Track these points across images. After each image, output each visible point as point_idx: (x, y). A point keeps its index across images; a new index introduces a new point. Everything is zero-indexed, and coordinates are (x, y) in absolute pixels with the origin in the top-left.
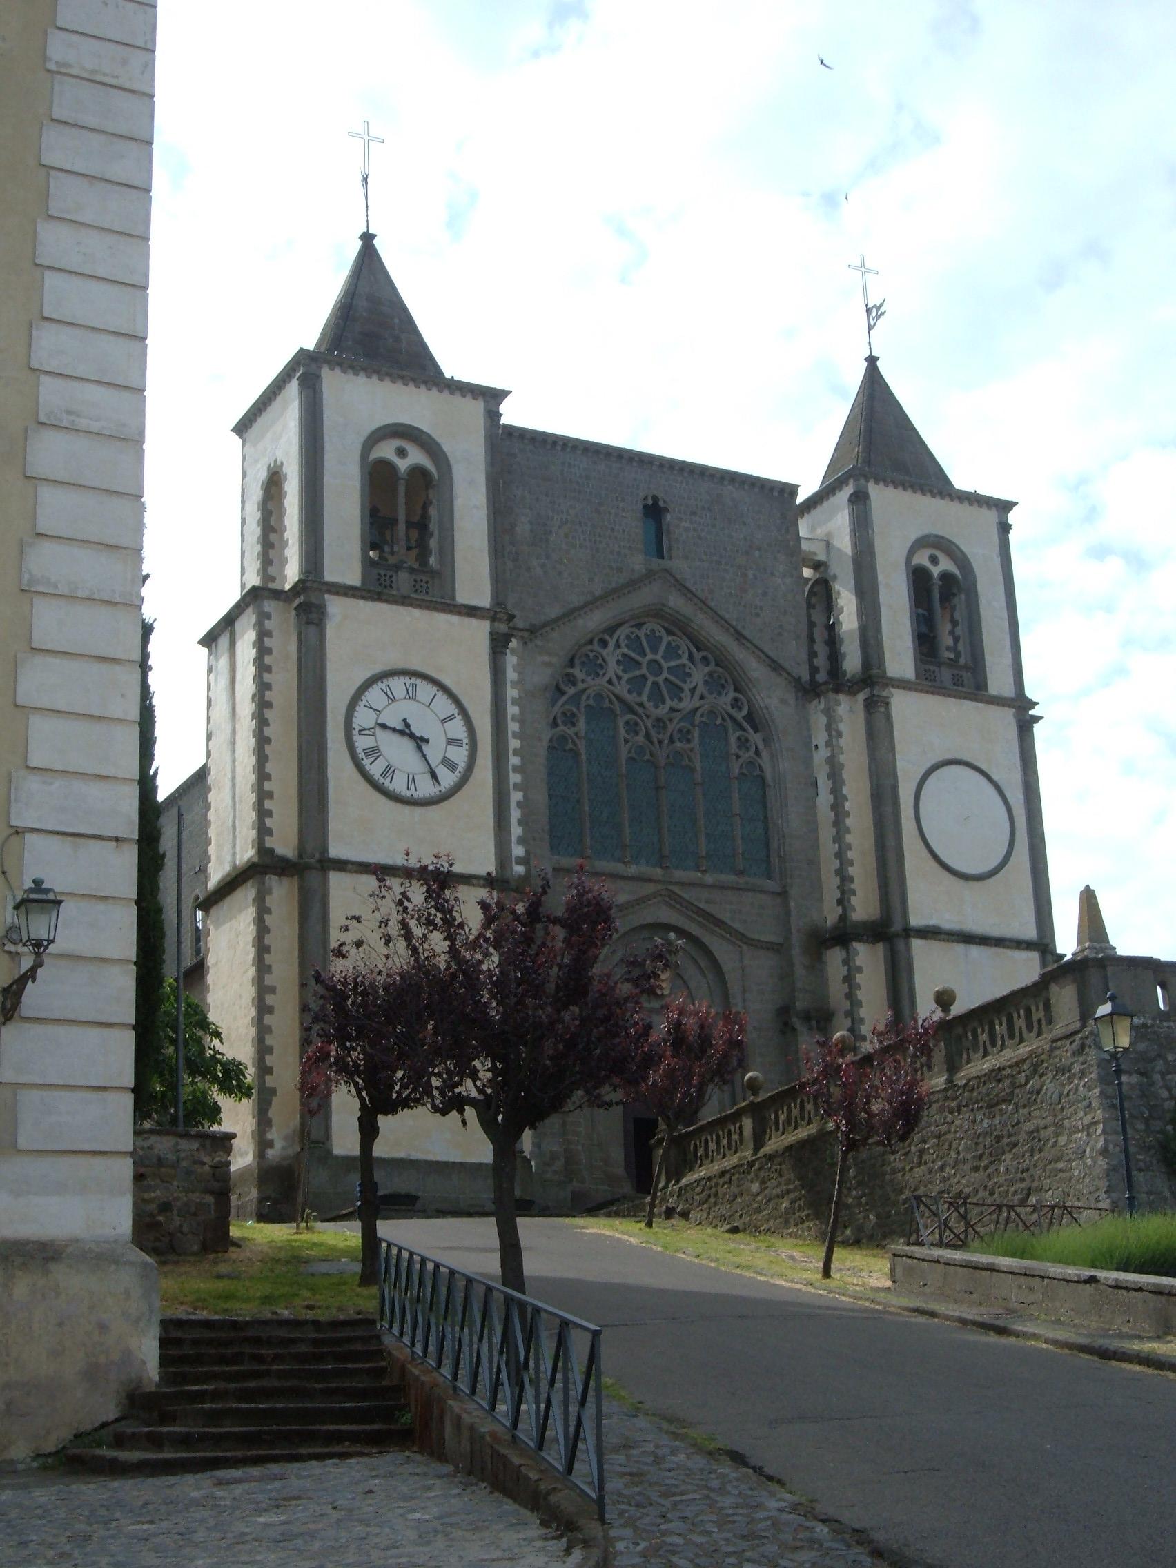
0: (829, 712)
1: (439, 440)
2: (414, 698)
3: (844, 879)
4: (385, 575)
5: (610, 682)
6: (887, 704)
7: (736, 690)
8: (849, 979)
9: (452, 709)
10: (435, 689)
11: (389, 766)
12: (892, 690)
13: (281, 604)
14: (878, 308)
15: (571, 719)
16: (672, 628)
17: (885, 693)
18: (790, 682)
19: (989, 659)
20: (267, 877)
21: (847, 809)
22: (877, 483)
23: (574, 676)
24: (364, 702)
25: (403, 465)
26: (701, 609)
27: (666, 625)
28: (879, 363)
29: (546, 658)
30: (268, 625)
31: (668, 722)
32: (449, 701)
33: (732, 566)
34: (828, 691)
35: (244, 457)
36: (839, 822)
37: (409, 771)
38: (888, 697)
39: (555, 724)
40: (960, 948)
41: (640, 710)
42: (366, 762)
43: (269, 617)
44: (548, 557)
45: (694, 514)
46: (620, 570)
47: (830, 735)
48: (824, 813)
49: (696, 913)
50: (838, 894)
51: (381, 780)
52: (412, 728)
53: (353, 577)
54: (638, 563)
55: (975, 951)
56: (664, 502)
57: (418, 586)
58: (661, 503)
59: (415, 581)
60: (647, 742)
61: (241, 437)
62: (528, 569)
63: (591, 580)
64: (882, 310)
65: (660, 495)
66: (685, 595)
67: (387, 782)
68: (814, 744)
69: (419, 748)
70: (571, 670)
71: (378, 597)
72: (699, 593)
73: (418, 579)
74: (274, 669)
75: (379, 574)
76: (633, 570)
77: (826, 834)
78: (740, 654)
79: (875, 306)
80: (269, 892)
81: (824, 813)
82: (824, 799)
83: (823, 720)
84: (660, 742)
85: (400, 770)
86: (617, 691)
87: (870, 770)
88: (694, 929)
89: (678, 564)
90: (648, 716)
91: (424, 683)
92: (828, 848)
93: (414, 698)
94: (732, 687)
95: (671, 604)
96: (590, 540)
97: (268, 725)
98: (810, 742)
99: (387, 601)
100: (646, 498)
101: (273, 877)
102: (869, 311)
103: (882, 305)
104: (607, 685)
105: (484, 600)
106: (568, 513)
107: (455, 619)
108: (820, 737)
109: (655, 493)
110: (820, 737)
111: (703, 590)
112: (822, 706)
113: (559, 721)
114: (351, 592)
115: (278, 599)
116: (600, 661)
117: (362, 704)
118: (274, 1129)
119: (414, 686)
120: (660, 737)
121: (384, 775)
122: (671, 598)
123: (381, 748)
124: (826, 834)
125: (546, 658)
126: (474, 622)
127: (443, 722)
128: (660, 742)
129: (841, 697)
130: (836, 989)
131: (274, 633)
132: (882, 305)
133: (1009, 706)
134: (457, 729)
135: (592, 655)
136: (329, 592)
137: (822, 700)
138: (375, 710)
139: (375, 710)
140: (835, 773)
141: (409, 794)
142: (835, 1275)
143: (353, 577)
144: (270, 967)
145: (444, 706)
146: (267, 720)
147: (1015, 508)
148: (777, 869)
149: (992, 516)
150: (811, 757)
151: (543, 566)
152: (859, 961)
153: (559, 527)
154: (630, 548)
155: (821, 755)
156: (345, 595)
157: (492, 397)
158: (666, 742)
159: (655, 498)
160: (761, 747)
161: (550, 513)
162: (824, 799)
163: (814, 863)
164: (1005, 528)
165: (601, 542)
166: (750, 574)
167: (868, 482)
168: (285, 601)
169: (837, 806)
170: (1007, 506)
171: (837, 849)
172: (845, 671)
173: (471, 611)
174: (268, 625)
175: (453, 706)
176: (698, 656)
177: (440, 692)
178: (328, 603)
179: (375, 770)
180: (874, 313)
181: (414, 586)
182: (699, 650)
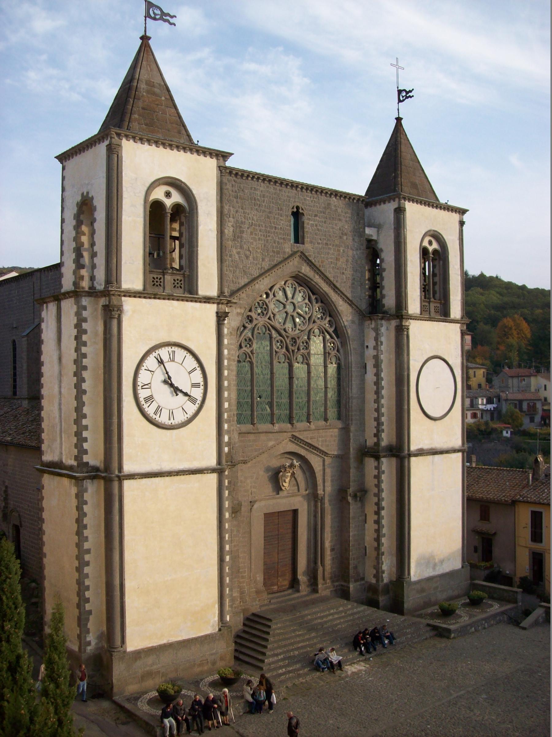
0: (377, 330)
1: (191, 187)
2: (173, 361)
3: (379, 424)
4: (157, 278)
5: (269, 318)
6: (408, 329)
7: (330, 316)
8: (378, 477)
9: (195, 364)
10: (186, 352)
11: (159, 407)
12: (411, 321)
13: (93, 298)
14: (407, 92)
15: (249, 341)
16: (300, 283)
17: (407, 324)
18: (357, 311)
19: (452, 297)
20: (85, 481)
21: (383, 385)
22: (409, 202)
23: (251, 317)
24: (145, 367)
25: (168, 203)
26: (317, 273)
27: (298, 281)
28: (403, 122)
29: (239, 310)
30: (85, 314)
31: (297, 339)
32: (193, 359)
33: (333, 245)
34: (377, 319)
35: (63, 178)
36: (377, 392)
37: (170, 409)
38: (409, 326)
39: (241, 347)
40: (430, 458)
41: (283, 333)
42: (145, 406)
43: (85, 308)
44: (241, 247)
45: (316, 216)
46: (278, 253)
47: (377, 344)
48: (370, 387)
49: (305, 445)
50: (375, 431)
51: (154, 417)
52: (172, 379)
53: (138, 286)
54: (289, 246)
55: (437, 457)
56: (302, 209)
57: (176, 284)
58: (301, 211)
59: (174, 280)
60: (287, 353)
61: (62, 163)
62: (231, 256)
63: (263, 260)
64: (410, 94)
65: (300, 205)
66: (310, 266)
67: (157, 417)
68: (366, 344)
69: (169, 378)
70: (250, 314)
71: (155, 296)
72: (316, 264)
73: (176, 279)
74: (88, 344)
75: (154, 278)
76: (284, 252)
77: (370, 396)
78: (334, 297)
79: (405, 90)
80: (86, 490)
81: (370, 387)
82: (370, 377)
83: (373, 334)
84: (293, 351)
85: (164, 408)
86: (272, 324)
87: (396, 364)
88: (302, 452)
89: (308, 247)
90: (287, 337)
91: (180, 349)
92: (370, 405)
93: (173, 361)
94: (320, 301)
95: (303, 271)
96: (264, 236)
97: (84, 381)
98: (364, 344)
99: (159, 298)
100: (293, 208)
101: (88, 480)
102: (400, 92)
103: (410, 91)
104: (268, 321)
105: (213, 292)
106: (253, 219)
107: (198, 305)
108: (371, 343)
109: (298, 204)
110: (371, 343)
111: (319, 261)
112: (373, 326)
113: (243, 345)
114: (138, 295)
115: (91, 296)
116: (265, 306)
117: (143, 368)
118: (91, 634)
119: (174, 352)
120: (293, 348)
121: (155, 413)
122: (303, 267)
123: (154, 396)
124: (370, 396)
125: (239, 310)
126: (208, 305)
127: (190, 373)
128: (293, 351)
129: (383, 322)
130: (370, 482)
131: (88, 319)
132: (410, 91)
133: (458, 323)
134: (198, 377)
135: (261, 302)
136: (125, 296)
137: (373, 322)
138: (151, 371)
139: (151, 371)
140: (377, 366)
141: (170, 422)
142: (300, 491)
143: (138, 286)
144: (87, 537)
145: (191, 363)
146: (84, 378)
147: (467, 212)
148: (344, 414)
149: (456, 217)
150: (364, 352)
151: (238, 253)
152: (384, 468)
153: (248, 228)
154: (284, 239)
155: (370, 352)
156: (135, 297)
157: (223, 156)
158: (296, 351)
159: (298, 208)
160: (340, 346)
161: (243, 220)
162: (370, 377)
163: (362, 411)
164: (462, 223)
165: (269, 236)
166: (342, 250)
167: (405, 201)
168: (95, 297)
169: (377, 383)
170: (463, 212)
171: (376, 407)
172: (384, 305)
173: (207, 300)
174: (85, 314)
175: (196, 362)
176: (313, 297)
177: (189, 354)
178: (124, 303)
179: (150, 410)
180: (404, 94)
181: (174, 284)
182: (313, 294)
